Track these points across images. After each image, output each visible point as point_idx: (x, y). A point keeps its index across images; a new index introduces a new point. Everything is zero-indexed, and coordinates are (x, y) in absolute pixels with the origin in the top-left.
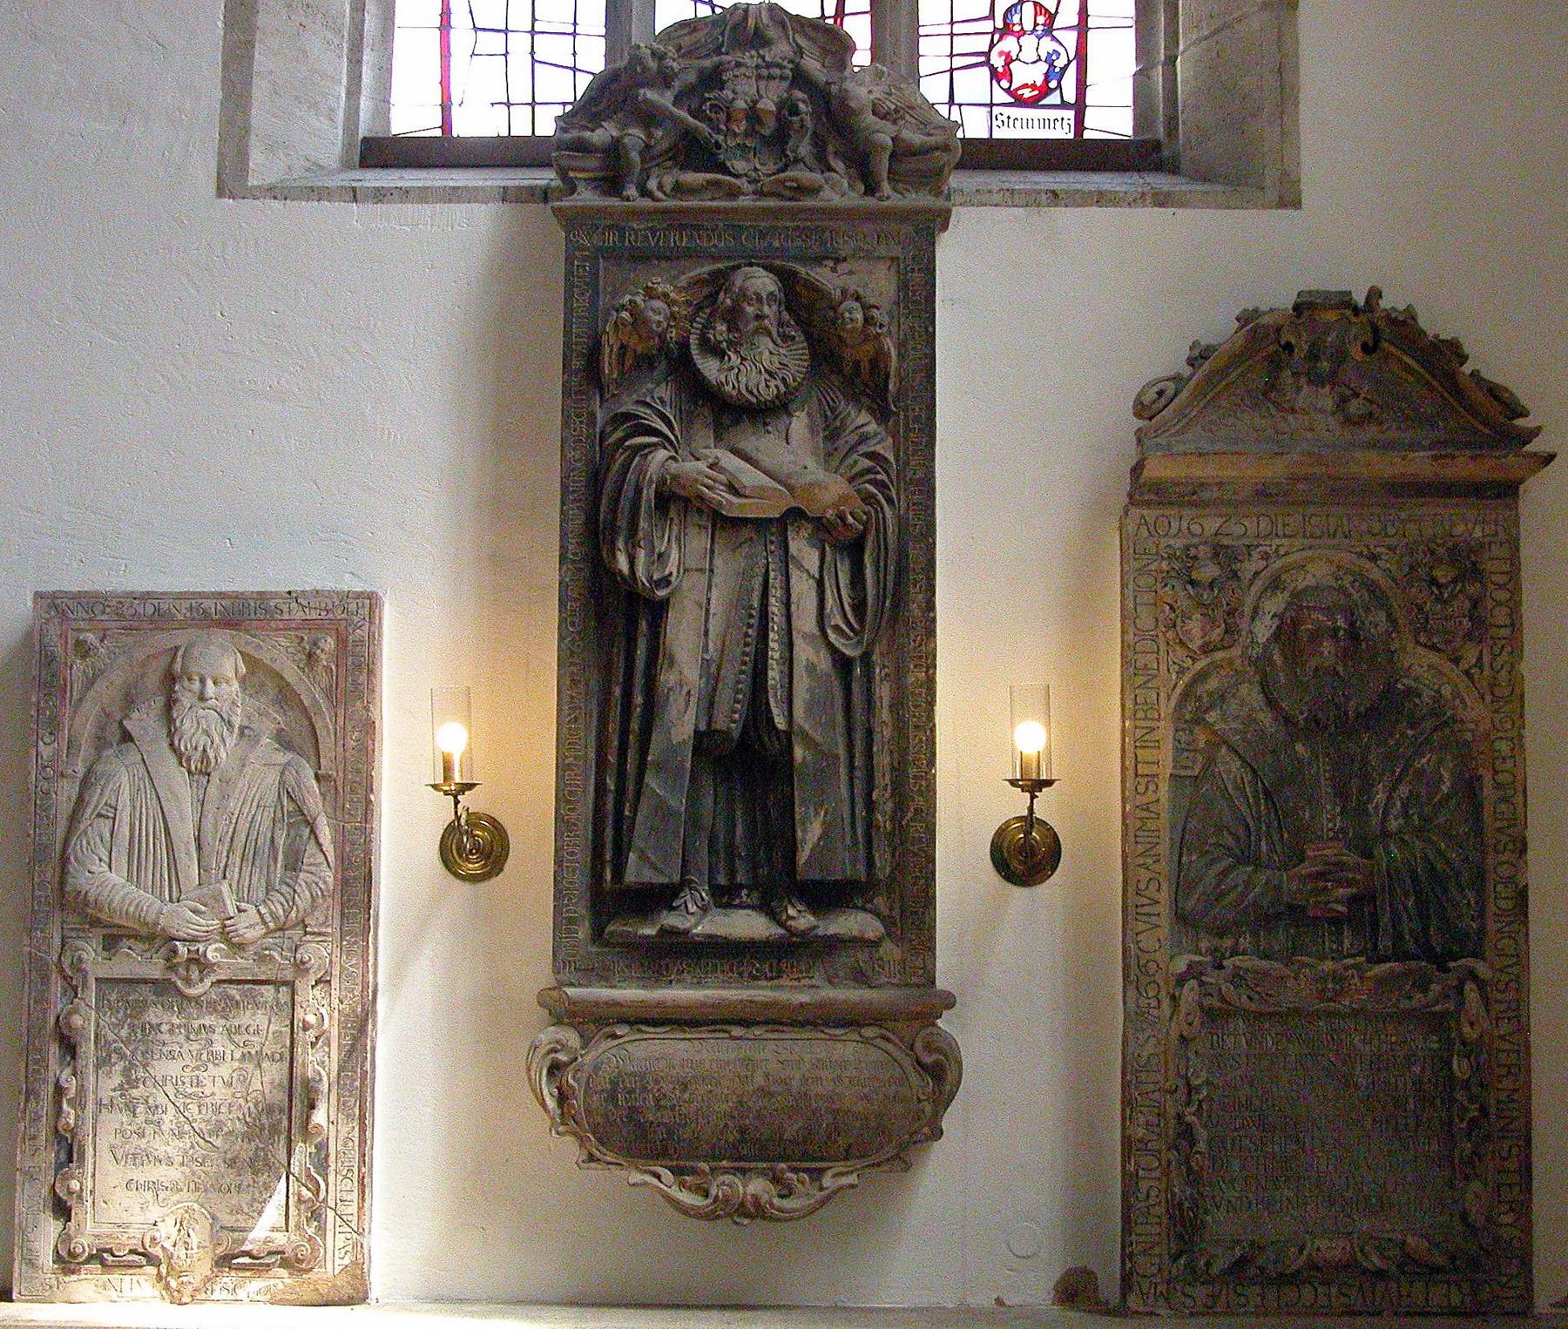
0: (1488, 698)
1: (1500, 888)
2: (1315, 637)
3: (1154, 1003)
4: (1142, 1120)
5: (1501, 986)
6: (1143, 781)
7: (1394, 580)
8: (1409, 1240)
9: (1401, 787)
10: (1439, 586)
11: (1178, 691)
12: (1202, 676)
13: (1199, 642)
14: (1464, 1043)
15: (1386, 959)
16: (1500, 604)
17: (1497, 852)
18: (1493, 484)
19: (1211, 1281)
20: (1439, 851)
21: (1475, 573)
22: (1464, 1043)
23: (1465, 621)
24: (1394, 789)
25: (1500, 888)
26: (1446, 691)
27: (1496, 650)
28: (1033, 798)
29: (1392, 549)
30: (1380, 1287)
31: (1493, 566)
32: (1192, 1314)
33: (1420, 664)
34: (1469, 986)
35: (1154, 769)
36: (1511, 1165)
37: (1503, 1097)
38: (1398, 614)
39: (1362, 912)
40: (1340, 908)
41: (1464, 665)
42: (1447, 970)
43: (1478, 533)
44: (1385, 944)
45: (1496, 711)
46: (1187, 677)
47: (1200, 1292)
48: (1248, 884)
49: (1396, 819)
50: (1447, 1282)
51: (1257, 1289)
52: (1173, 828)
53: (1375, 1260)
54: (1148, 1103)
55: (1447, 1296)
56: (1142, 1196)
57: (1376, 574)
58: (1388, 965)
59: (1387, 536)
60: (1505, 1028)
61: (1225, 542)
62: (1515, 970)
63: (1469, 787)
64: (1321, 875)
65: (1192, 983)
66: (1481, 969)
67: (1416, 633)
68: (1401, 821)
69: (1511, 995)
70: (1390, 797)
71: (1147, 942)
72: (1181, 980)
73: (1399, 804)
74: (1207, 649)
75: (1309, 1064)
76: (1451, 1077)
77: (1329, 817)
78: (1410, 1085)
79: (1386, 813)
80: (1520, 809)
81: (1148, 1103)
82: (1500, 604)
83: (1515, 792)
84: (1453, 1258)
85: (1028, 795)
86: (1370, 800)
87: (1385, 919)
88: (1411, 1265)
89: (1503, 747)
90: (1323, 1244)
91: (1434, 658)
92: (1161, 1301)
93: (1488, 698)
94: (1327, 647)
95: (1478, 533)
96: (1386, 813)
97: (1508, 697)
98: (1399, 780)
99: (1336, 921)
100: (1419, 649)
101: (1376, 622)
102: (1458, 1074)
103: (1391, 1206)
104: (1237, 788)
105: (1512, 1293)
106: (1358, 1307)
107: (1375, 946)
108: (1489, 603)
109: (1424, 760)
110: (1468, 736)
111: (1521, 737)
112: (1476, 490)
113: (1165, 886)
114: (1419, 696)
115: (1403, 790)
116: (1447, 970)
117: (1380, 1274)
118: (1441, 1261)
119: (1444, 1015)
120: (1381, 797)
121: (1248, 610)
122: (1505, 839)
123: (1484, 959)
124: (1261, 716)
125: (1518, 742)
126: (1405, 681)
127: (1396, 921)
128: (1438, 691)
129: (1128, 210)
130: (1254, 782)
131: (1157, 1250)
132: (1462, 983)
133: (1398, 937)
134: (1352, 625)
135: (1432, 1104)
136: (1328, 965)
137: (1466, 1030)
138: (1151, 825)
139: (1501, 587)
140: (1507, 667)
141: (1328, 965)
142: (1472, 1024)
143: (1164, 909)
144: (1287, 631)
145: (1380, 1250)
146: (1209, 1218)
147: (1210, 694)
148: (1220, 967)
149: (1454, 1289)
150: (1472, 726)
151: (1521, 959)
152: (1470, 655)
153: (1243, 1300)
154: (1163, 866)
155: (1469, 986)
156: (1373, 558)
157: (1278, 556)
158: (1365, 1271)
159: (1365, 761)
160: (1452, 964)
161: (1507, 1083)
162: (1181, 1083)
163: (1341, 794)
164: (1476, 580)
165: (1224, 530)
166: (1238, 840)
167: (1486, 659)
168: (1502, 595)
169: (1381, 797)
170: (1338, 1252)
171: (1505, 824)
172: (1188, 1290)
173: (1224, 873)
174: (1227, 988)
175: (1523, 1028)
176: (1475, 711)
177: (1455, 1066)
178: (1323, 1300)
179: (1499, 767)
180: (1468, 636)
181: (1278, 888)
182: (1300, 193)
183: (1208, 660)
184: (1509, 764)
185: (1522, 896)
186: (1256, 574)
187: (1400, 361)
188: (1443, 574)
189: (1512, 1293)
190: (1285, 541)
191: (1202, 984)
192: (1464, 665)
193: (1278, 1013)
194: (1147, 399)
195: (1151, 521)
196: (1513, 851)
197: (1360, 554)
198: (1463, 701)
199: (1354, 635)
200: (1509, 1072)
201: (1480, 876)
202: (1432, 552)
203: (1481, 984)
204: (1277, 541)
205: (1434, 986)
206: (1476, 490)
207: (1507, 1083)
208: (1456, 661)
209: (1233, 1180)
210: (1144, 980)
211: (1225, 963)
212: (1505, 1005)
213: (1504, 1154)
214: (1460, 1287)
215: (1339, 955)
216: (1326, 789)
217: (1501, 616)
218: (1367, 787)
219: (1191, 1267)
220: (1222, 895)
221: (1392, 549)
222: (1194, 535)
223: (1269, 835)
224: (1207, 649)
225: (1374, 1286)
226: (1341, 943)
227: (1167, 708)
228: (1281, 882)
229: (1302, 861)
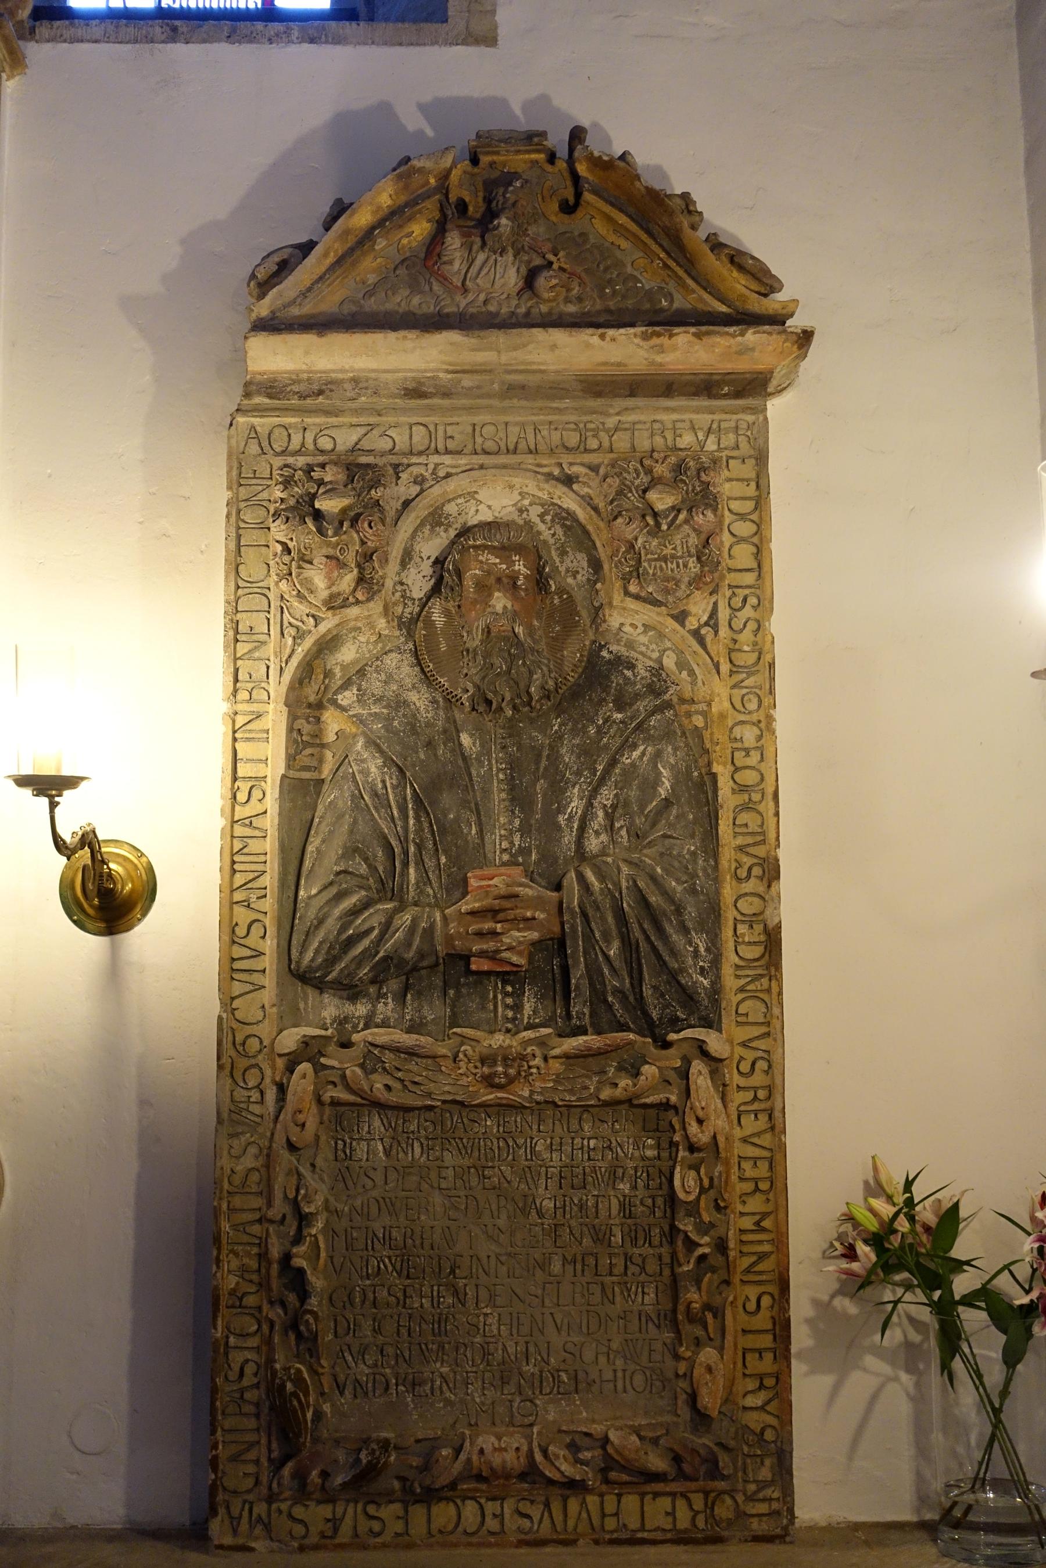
0: (725, 667)
1: (742, 929)
2: (483, 588)
3: (255, 1096)
4: (235, 1263)
5: (745, 1067)
6: (244, 787)
7: (596, 509)
8: (613, 1436)
9: (604, 791)
10: (655, 515)
11: (294, 662)
12: (327, 645)
13: (324, 594)
14: (692, 1148)
15: (582, 1031)
16: (741, 540)
17: (739, 880)
18: (728, 378)
19: (329, 1499)
20: (653, 878)
21: (705, 498)
22: (692, 1148)
23: (692, 562)
24: (595, 792)
25: (742, 929)
26: (669, 661)
27: (737, 602)
28: (53, 805)
29: (594, 468)
30: (573, 1505)
31: (729, 487)
32: (302, 1549)
33: (631, 625)
34: (698, 1066)
35: (259, 770)
36: (763, 1320)
37: (747, 1223)
38: (603, 553)
39: (553, 966)
40: (515, 959)
41: (692, 623)
42: (667, 1045)
43: (711, 446)
44: (580, 1008)
45: (733, 687)
46: (308, 643)
47: (317, 1514)
48: (386, 927)
49: (597, 833)
50: (673, 1495)
51: (396, 1508)
52: (283, 849)
53: (564, 1467)
54: (246, 1238)
55: (672, 1514)
56: (233, 1375)
57: (569, 502)
58: (582, 1039)
59: (586, 451)
60: (750, 1125)
61: (363, 460)
62: (762, 1044)
63: (702, 790)
64: (492, 913)
65: (305, 1067)
66: (715, 1043)
67: (626, 579)
68: (604, 837)
69: (758, 1079)
70: (590, 805)
71: (248, 1009)
72: (292, 1062)
73: (601, 814)
74: (335, 603)
75: (474, 1181)
76: (672, 1198)
77: (502, 834)
78: (615, 1210)
79: (582, 829)
80: (771, 821)
81: (246, 1238)
82: (741, 540)
83: (761, 797)
84: (677, 1459)
85: (45, 801)
86: (560, 811)
87: (578, 973)
88: (618, 1472)
89: (749, 735)
90: (487, 1441)
91: (648, 614)
92: (258, 1530)
93: (725, 667)
94: (500, 601)
95: (711, 446)
96: (582, 829)
97: (754, 670)
98: (602, 781)
99: (510, 976)
100: (631, 604)
101: (570, 569)
102: (681, 1195)
103: (590, 1384)
104: (375, 794)
105: (763, 1508)
106: (545, 1530)
107: (568, 1016)
108: (726, 539)
109: (636, 754)
110: (699, 721)
111: (770, 719)
112: (706, 387)
113: (271, 931)
114: (632, 667)
115: (607, 795)
116: (667, 1045)
117: (573, 1486)
118: (657, 1463)
119: (666, 1106)
120: (576, 805)
121: (396, 553)
122: (747, 861)
123: (720, 1030)
124: (413, 697)
125: (766, 727)
126: (614, 648)
127: (593, 974)
128: (659, 661)
129: (267, 46)
130: (400, 787)
131: (252, 1455)
132: (687, 1061)
133: (598, 998)
134: (540, 571)
135: (648, 1239)
136: (499, 1040)
137: (693, 1128)
138: (254, 846)
139: (742, 517)
140: (752, 626)
141: (499, 1040)
142: (700, 1121)
143: (268, 962)
144: (444, 577)
145: (574, 1448)
146: (327, 1408)
147: (344, 667)
148: (346, 1045)
149: (681, 1503)
150: (703, 707)
151: (771, 1027)
152: (699, 608)
153: (376, 1526)
154: (269, 904)
155: (698, 1066)
156: (568, 481)
157: (438, 480)
158: (551, 1482)
159: (554, 757)
160: (672, 1037)
161: (755, 1204)
162: (287, 1209)
163: (519, 799)
164: (707, 506)
165: (365, 445)
166: (372, 868)
167: (724, 614)
168: (744, 529)
169: (576, 805)
170: (510, 1457)
171: (750, 840)
172: (298, 1511)
173: (355, 912)
174: (354, 1071)
175: (775, 1126)
176: (719, 693)
177: (677, 1183)
178: (492, 1524)
179: (740, 759)
180: (696, 582)
181: (429, 932)
182: (495, 27)
183: (336, 620)
184: (754, 759)
185: (772, 941)
186: (406, 504)
187: (609, 219)
188: (662, 500)
189: (763, 1508)
190: (447, 460)
191: (318, 1068)
192: (692, 623)
193: (430, 1108)
194: (261, 275)
195: (263, 431)
196: (761, 878)
197: (549, 476)
198: (692, 673)
199: (540, 581)
200: (757, 1189)
201: (713, 912)
202: (649, 471)
203: (714, 1062)
204: (435, 459)
205: (646, 1069)
206: (706, 387)
207: (755, 1204)
208: (681, 617)
209: (363, 1351)
210: (242, 1063)
211: (355, 1037)
212: (750, 1095)
213: (752, 1306)
214: (688, 1500)
215: (514, 1027)
216: (499, 796)
217: (743, 555)
218: (557, 790)
219: (301, 1476)
220: (350, 943)
221: (594, 468)
222: (322, 452)
223: (420, 862)
224: (335, 603)
225: (565, 1500)
226: (517, 1007)
227: (277, 688)
228: (432, 926)
229: (465, 894)
